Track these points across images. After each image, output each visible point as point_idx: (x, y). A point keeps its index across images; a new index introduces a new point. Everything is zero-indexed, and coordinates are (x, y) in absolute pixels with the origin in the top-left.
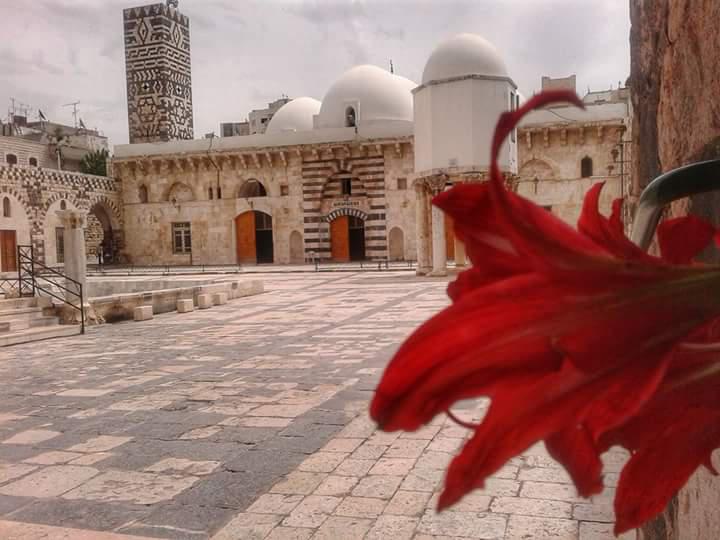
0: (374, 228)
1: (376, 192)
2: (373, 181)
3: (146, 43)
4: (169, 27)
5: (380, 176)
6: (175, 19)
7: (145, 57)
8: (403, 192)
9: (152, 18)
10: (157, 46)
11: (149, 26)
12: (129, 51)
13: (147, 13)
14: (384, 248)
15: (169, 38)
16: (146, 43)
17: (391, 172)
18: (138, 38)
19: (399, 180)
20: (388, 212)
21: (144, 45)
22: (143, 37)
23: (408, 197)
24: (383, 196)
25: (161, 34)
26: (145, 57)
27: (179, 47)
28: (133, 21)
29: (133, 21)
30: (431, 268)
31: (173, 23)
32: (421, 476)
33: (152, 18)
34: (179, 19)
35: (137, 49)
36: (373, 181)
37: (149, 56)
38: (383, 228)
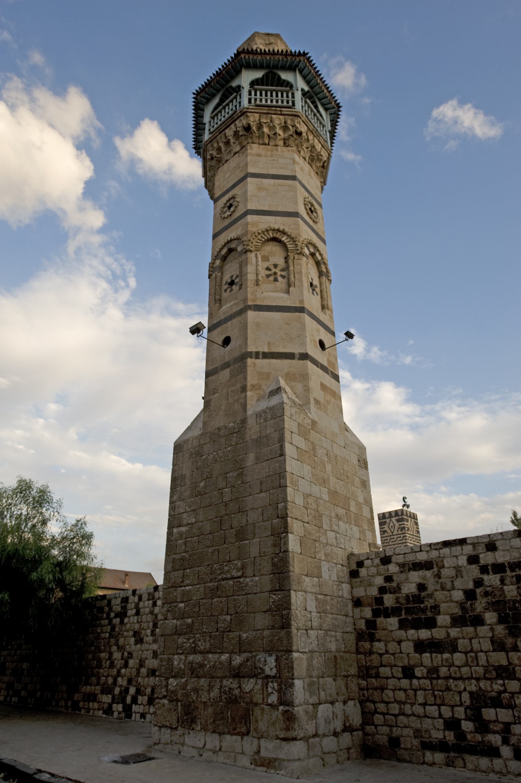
3: (394, 534)
4: (408, 522)
6: (410, 517)
7: (395, 543)
9: (397, 518)
10: (402, 535)
11: (395, 523)
12: (383, 539)
13: (393, 514)
15: (408, 530)
16: (394, 534)
18: (388, 530)
21: (393, 535)
22: (392, 530)
25: (404, 528)
26: (395, 543)
27: (414, 534)
28: (384, 520)
29: (384, 520)
31: (410, 519)
32: (259, 158)
33: (397, 518)
34: (409, 514)
35: (388, 538)
37: (397, 542)
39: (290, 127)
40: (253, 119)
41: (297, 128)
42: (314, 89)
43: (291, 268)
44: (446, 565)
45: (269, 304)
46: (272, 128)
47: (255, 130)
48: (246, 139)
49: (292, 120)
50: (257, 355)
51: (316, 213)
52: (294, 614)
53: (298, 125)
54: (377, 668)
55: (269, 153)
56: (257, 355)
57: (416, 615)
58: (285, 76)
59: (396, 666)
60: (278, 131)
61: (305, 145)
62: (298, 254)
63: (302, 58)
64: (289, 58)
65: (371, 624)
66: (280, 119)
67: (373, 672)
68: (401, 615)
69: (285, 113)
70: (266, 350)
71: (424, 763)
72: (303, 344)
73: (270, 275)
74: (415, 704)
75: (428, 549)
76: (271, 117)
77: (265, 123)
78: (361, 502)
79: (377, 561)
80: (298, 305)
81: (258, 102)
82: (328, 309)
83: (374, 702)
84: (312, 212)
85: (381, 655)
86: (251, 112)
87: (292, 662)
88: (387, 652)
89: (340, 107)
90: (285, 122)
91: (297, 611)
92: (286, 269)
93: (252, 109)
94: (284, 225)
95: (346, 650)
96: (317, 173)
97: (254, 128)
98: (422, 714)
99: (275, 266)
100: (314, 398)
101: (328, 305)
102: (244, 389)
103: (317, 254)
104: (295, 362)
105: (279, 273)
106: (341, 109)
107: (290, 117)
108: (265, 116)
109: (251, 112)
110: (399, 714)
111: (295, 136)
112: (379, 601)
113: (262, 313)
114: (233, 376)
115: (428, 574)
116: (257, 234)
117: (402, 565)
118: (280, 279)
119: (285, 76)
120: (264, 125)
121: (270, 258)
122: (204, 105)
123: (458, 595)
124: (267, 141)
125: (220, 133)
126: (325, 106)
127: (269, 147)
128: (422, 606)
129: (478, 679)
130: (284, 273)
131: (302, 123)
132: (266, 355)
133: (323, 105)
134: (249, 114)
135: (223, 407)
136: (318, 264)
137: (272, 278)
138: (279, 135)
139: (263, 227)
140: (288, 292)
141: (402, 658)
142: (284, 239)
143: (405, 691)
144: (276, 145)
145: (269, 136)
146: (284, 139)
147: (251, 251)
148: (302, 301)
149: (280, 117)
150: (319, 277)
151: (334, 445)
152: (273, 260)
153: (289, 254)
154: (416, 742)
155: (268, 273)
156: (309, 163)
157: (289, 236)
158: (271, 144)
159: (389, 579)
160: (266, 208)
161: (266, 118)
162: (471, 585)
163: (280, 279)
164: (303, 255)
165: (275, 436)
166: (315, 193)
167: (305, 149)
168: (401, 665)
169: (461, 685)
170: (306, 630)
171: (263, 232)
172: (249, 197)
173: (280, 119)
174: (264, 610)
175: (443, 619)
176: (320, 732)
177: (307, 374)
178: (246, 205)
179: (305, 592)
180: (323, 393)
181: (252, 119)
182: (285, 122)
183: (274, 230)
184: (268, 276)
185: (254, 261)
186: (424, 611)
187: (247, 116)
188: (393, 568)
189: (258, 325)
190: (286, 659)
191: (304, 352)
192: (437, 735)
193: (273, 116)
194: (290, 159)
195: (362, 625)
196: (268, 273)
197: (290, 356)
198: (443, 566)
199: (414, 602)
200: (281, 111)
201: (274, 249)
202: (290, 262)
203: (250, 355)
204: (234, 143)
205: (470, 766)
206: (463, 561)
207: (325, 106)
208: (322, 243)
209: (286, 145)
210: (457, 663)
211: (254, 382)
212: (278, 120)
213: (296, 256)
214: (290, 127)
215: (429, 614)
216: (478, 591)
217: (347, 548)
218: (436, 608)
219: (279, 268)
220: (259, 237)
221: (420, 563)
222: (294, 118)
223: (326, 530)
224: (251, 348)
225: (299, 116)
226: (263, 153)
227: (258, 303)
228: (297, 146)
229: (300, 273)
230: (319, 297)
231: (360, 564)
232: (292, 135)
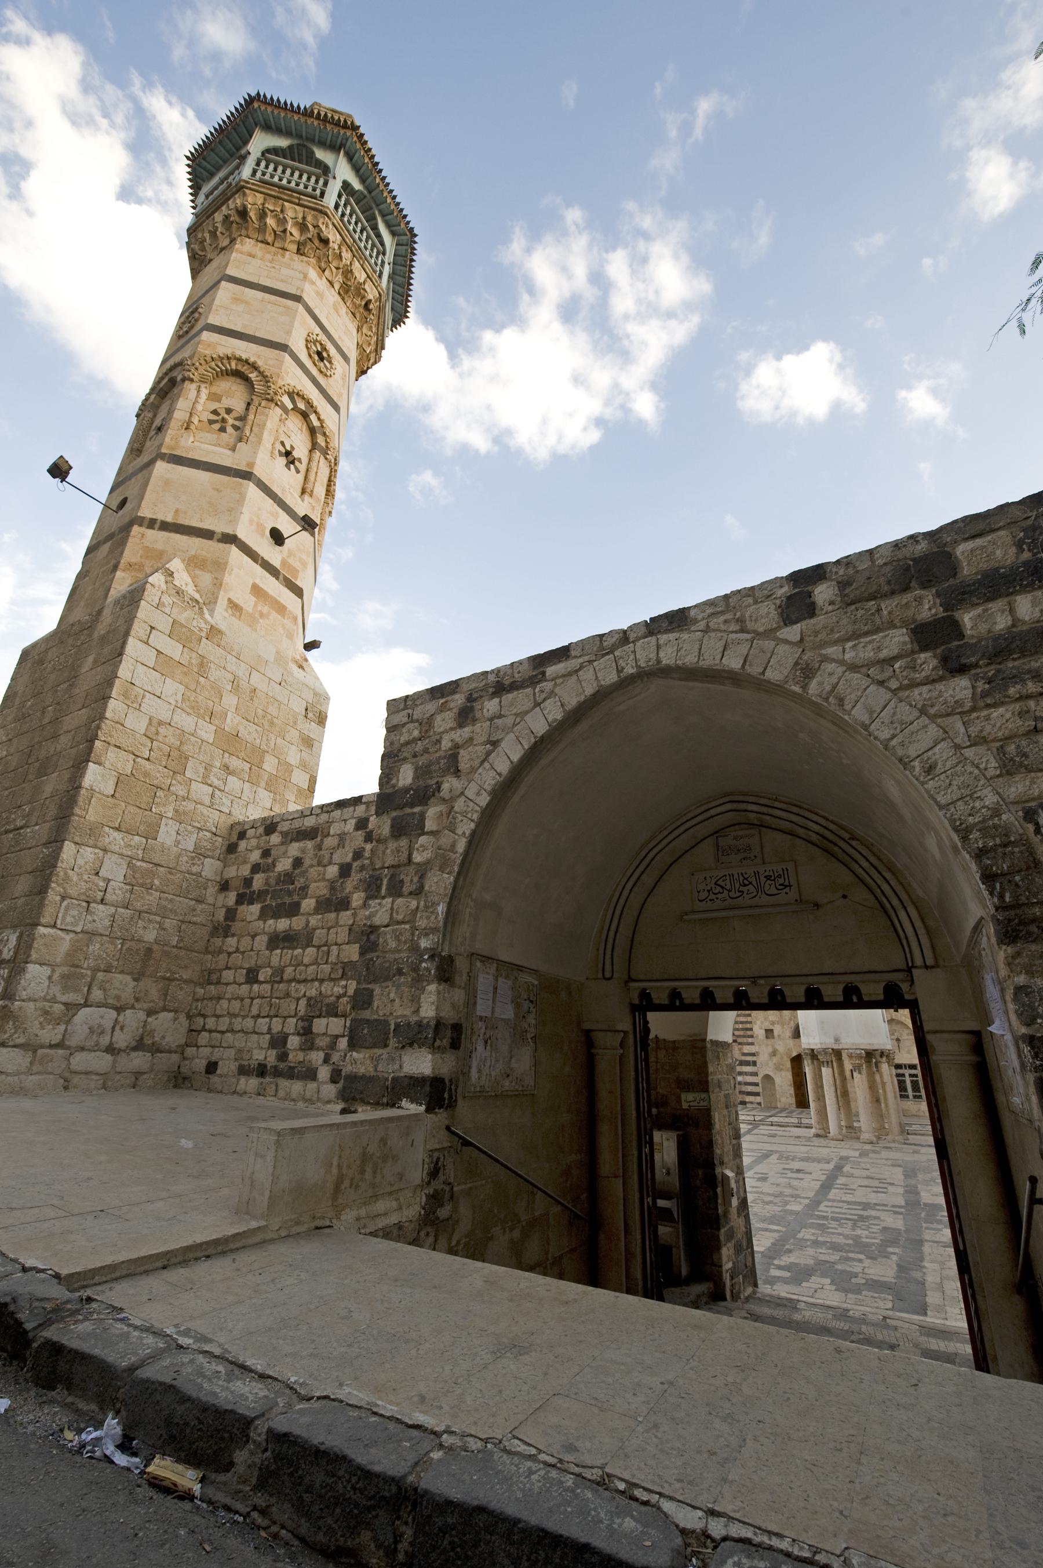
0: (746, 1074)
1: (745, 1040)
2: (743, 1029)
5: (748, 1026)
8: (770, 1042)
14: (757, 1094)
17: (758, 1022)
19: (766, 1030)
20: (760, 1060)
23: (777, 1047)
24: (752, 1044)
30: (826, 1130)
36: (743, 1029)
38: (756, 1074)
39: (311, 227)
40: (253, 200)
41: (321, 230)
42: (373, 194)
43: (251, 417)
44: (332, 832)
45: (196, 458)
46: (282, 221)
47: (253, 217)
48: (238, 229)
49: (315, 217)
50: (152, 524)
51: (330, 362)
52: (62, 874)
53: (323, 228)
54: (220, 971)
55: (268, 256)
56: (152, 524)
57: (281, 898)
58: (320, 154)
59: (241, 968)
60: (289, 228)
61: (335, 263)
62: (267, 399)
63: (349, 132)
64: (329, 127)
65: (231, 914)
66: (296, 211)
67: (214, 977)
68: (265, 900)
69: (306, 203)
70: (169, 519)
71: (235, 1092)
72: (234, 521)
73: (216, 422)
74: (247, 1016)
75: (319, 811)
76: (283, 205)
77: (272, 211)
78: (293, 762)
79: (261, 830)
80: (243, 467)
81: (267, 177)
82: (311, 496)
83: (204, 1016)
84: (322, 359)
85: (229, 954)
86: (251, 189)
87: (33, 940)
88: (237, 951)
89: (416, 235)
90: (304, 218)
91: (70, 872)
92: (242, 419)
93: (253, 184)
94: (259, 356)
95: (181, 945)
96: (354, 314)
97: (252, 214)
98: (251, 1030)
99: (229, 411)
100: (229, 599)
101: (312, 491)
102: (115, 568)
103: (313, 417)
104: (212, 545)
105: (231, 421)
106: (416, 239)
107: (313, 212)
108: (273, 200)
109: (251, 189)
110: (227, 1031)
111: (316, 242)
112: (248, 882)
113: (180, 467)
114: (111, 551)
115: (309, 844)
116: (208, 359)
117: (285, 834)
118: (229, 429)
119: (320, 154)
120: (269, 213)
121: (224, 398)
122: (204, 181)
123: (332, 871)
124: (270, 239)
125: (208, 218)
126: (394, 228)
127: (273, 249)
128: (291, 887)
129: (322, 981)
130: (237, 423)
131: (331, 226)
132: (165, 526)
133: (389, 225)
134: (247, 191)
135: (86, 595)
136: (312, 431)
137: (217, 426)
138: (291, 234)
139: (222, 351)
140: (233, 449)
141: (251, 957)
142: (253, 376)
143: (242, 999)
144: (284, 249)
145: (275, 232)
146: (299, 243)
147: (192, 380)
148: (251, 465)
149: (297, 207)
150: (310, 451)
151: (254, 673)
152: (226, 402)
153: (254, 397)
154: (234, 1066)
155: (214, 417)
156: (339, 293)
157: (261, 373)
158: (276, 245)
159: (266, 853)
160: (238, 328)
161: (275, 204)
162: (349, 858)
163: (229, 429)
164: (277, 404)
165: (122, 629)
166: (340, 338)
167: (334, 270)
168: (247, 966)
169: (302, 988)
170: (88, 902)
171: (221, 359)
172: (214, 307)
173: (296, 211)
174: (30, 870)
175: (308, 904)
176: (73, 1042)
177: (226, 564)
178: (207, 317)
179: (105, 851)
180: (254, 599)
181: (250, 199)
182: (304, 218)
183: (239, 360)
184: (211, 422)
185: (192, 394)
186: (290, 893)
187: (244, 194)
188: (275, 839)
189: (167, 483)
190: (28, 936)
191: (231, 532)
192: (259, 1056)
193: (286, 204)
194: (300, 272)
195: (221, 915)
196: (214, 417)
197: (207, 534)
198: (328, 834)
199: (284, 882)
200: (299, 199)
201: (234, 387)
202: (252, 409)
203: (140, 521)
204: (223, 234)
205: (281, 1093)
206: (351, 825)
207: (394, 228)
208: (329, 408)
209: (299, 252)
210: (306, 960)
211: (133, 560)
212: (292, 212)
213: (264, 403)
214: (311, 227)
215: (296, 898)
216: (355, 864)
217: (234, 813)
218: (304, 888)
219: (234, 414)
220: (213, 364)
221: (306, 831)
222: (319, 215)
223: (191, 780)
224: (146, 511)
225: (326, 214)
226: (259, 254)
227: (178, 452)
228: (319, 260)
229: (263, 426)
230: (300, 477)
231: (242, 835)
232: (310, 239)
